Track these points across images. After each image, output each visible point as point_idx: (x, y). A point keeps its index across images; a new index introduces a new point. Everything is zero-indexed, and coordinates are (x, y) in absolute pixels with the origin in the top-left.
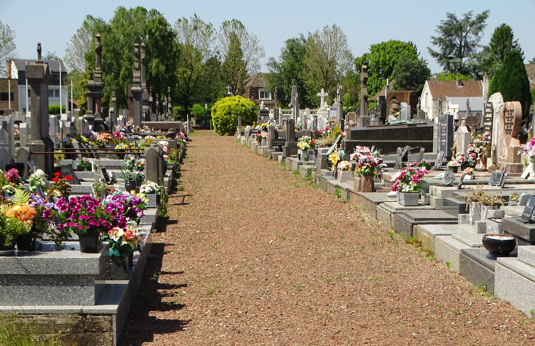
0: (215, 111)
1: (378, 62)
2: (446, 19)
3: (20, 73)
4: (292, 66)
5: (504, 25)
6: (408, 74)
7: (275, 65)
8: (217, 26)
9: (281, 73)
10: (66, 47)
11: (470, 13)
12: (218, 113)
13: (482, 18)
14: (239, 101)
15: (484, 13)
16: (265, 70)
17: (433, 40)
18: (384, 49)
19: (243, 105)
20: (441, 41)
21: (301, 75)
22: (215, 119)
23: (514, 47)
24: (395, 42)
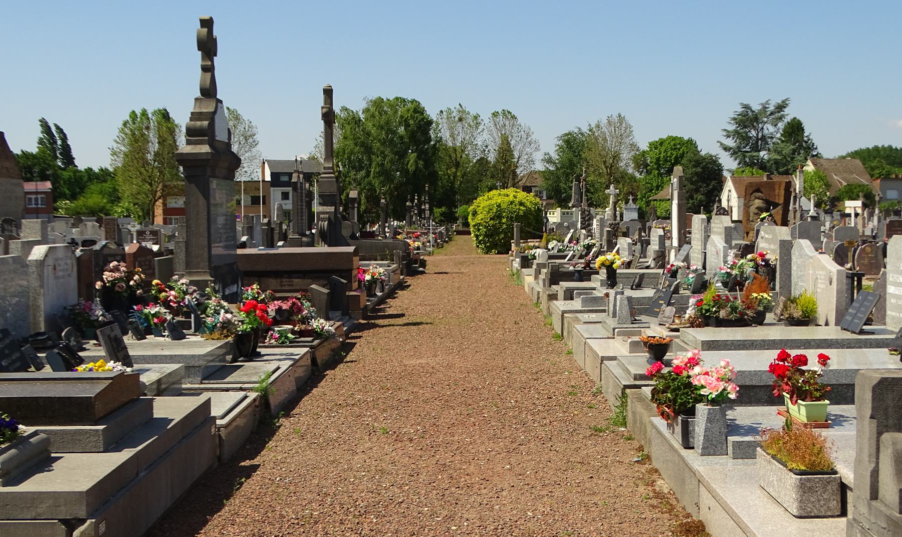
0: (475, 213)
1: (658, 159)
2: (740, 110)
3: (273, 175)
4: (570, 161)
5: (795, 118)
6: (699, 169)
7: (549, 161)
8: (486, 118)
9: (557, 168)
10: (315, 143)
11: (767, 103)
12: (480, 217)
13: (781, 107)
14: (515, 197)
15: (783, 102)
16: (539, 166)
17: (725, 133)
18: (661, 144)
19: (521, 204)
20: (736, 133)
21: (579, 173)
22: (474, 226)
23: (806, 142)
24: (674, 139)
